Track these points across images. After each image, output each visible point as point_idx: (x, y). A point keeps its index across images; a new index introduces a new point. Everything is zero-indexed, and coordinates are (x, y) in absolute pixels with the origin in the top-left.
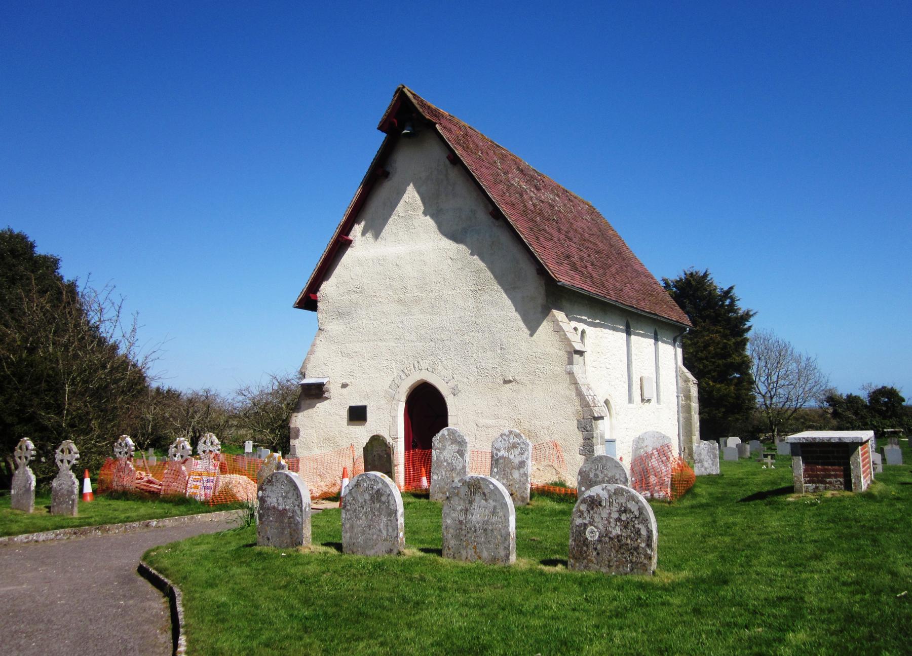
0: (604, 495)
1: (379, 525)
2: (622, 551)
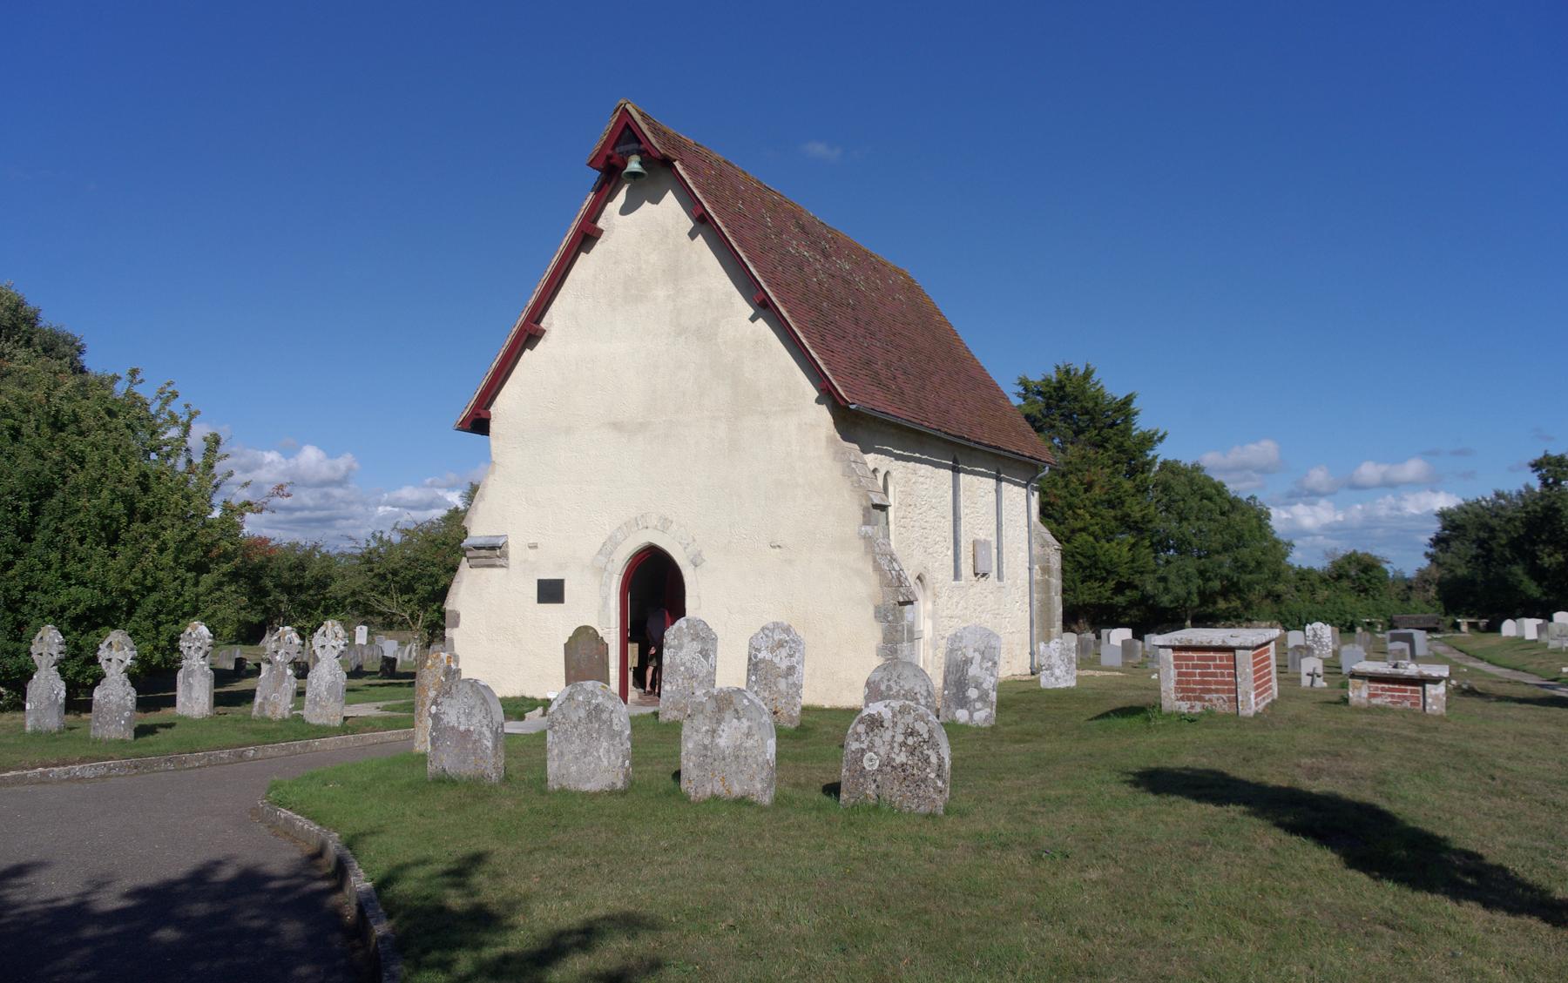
0: (887, 714)
1: (598, 751)
2: (907, 783)
